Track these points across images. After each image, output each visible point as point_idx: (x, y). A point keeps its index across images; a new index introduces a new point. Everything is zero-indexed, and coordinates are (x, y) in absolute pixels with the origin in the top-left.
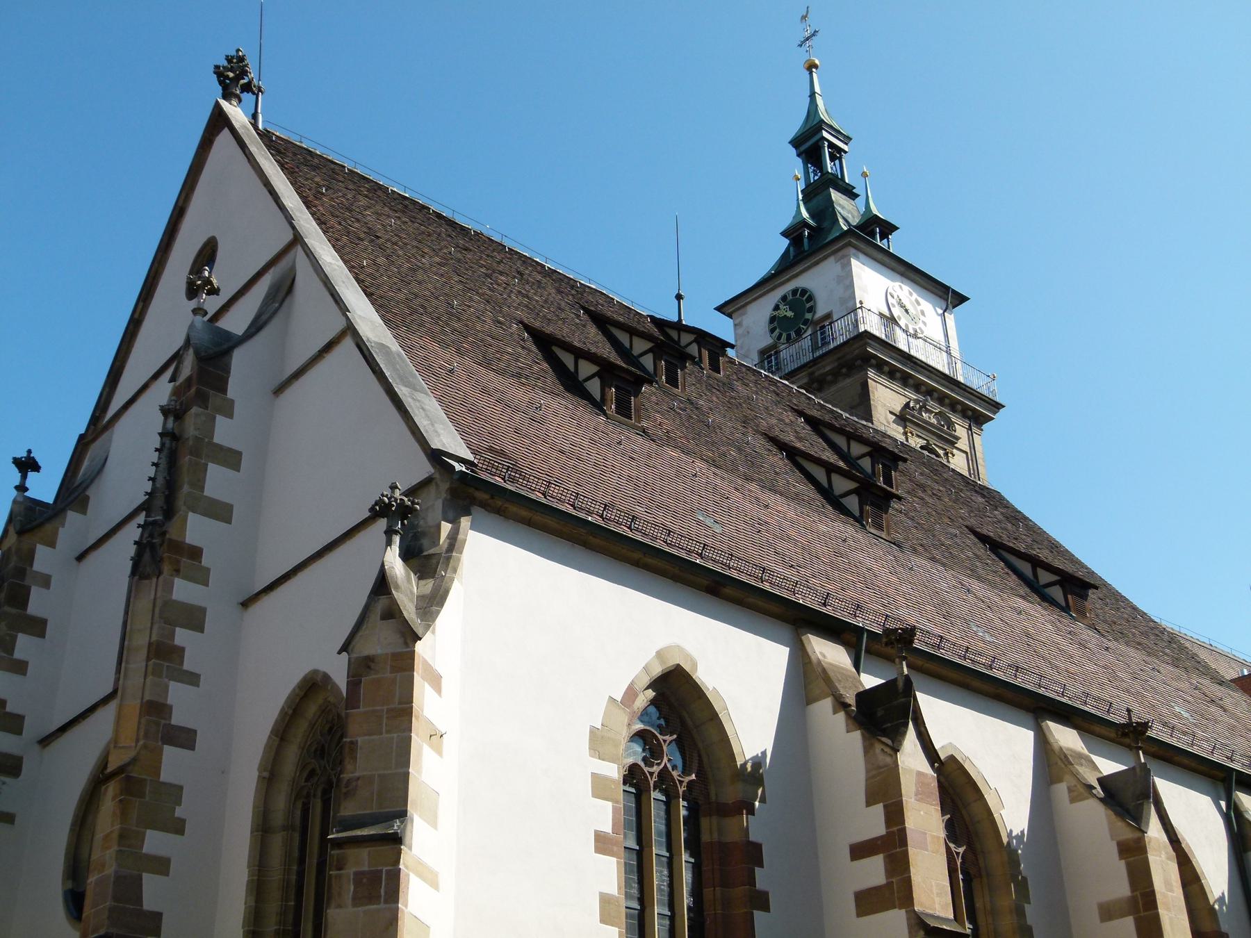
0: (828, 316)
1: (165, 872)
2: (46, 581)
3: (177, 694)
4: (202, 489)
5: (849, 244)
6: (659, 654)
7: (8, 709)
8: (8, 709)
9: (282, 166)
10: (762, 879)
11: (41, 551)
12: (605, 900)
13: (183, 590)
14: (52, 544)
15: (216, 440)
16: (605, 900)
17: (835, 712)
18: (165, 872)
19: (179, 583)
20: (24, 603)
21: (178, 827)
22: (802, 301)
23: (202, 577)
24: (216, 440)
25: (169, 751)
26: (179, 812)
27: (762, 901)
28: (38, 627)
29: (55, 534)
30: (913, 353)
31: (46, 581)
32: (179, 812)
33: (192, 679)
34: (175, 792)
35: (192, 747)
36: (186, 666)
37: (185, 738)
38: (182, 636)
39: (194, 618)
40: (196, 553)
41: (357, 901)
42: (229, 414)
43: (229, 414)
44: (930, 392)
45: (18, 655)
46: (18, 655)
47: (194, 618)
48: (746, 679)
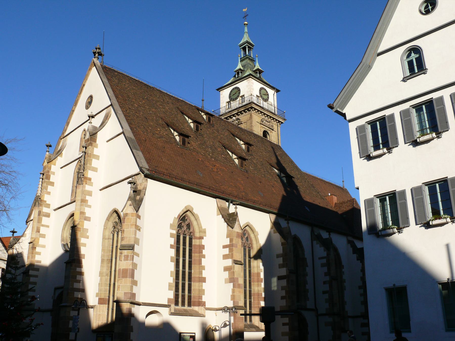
0: (243, 96)
1: (85, 246)
2: (54, 173)
3: (87, 210)
4: (91, 165)
5: (250, 77)
6: (186, 207)
7: (47, 203)
8: (47, 203)
9: (127, 120)
10: (204, 252)
11: (53, 167)
12: (172, 257)
13: (88, 188)
14: (55, 165)
15: (94, 153)
16: (172, 257)
17: (218, 215)
18: (85, 246)
19: (87, 186)
20: (49, 179)
21: (88, 237)
22: (238, 89)
23: (91, 185)
24: (94, 153)
25: (86, 222)
26: (88, 234)
27: (204, 256)
28: (52, 184)
29: (55, 163)
30: (264, 107)
31: (54, 173)
32: (88, 234)
33: (90, 206)
34: (87, 230)
35: (90, 221)
36: (88, 204)
37: (88, 219)
38: (88, 198)
39: (90, 194)
40: (90, 179)
41: (125, 260)
42: (97, 147)
43: (97, 147)
44: (268, 116)
45: (48, 191)
46: (48, 191)
47: (90, 194)
48: (206, 209)
